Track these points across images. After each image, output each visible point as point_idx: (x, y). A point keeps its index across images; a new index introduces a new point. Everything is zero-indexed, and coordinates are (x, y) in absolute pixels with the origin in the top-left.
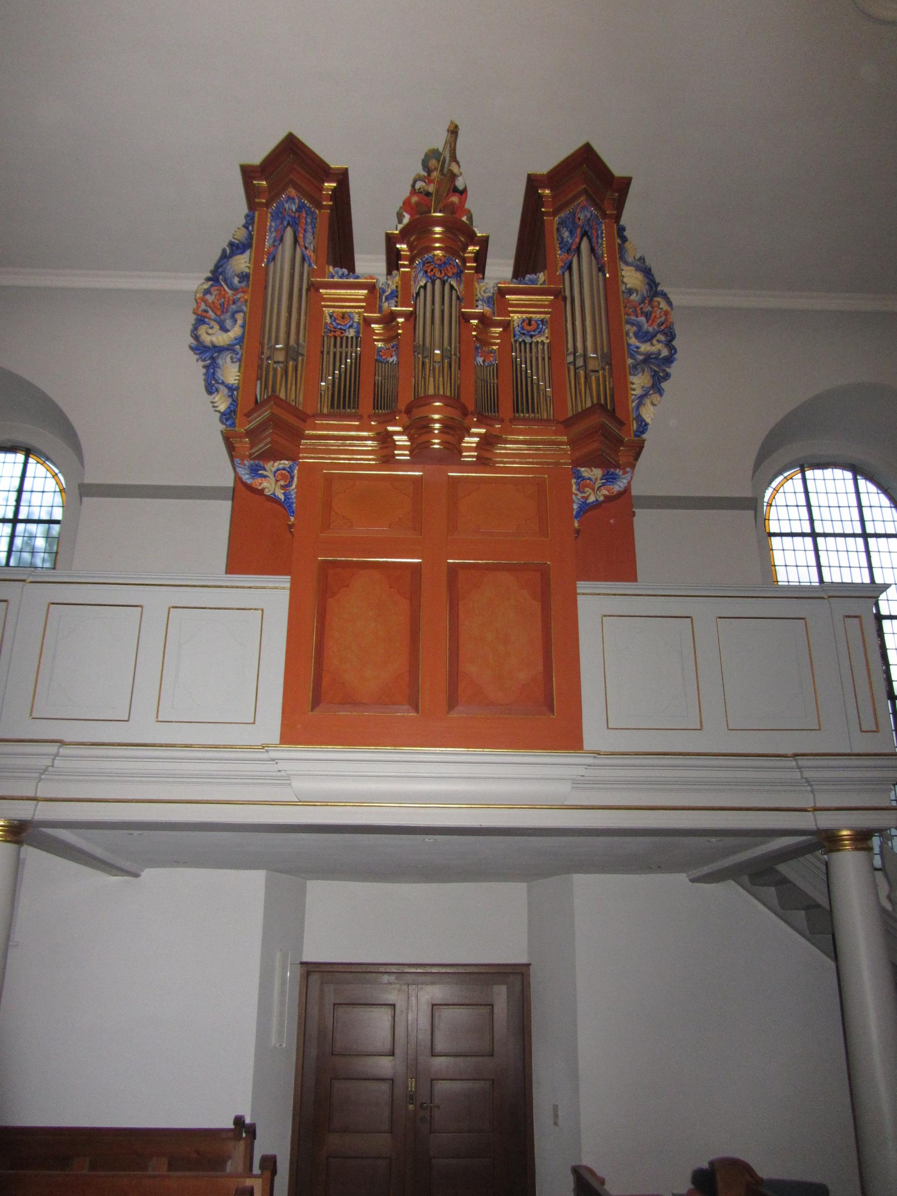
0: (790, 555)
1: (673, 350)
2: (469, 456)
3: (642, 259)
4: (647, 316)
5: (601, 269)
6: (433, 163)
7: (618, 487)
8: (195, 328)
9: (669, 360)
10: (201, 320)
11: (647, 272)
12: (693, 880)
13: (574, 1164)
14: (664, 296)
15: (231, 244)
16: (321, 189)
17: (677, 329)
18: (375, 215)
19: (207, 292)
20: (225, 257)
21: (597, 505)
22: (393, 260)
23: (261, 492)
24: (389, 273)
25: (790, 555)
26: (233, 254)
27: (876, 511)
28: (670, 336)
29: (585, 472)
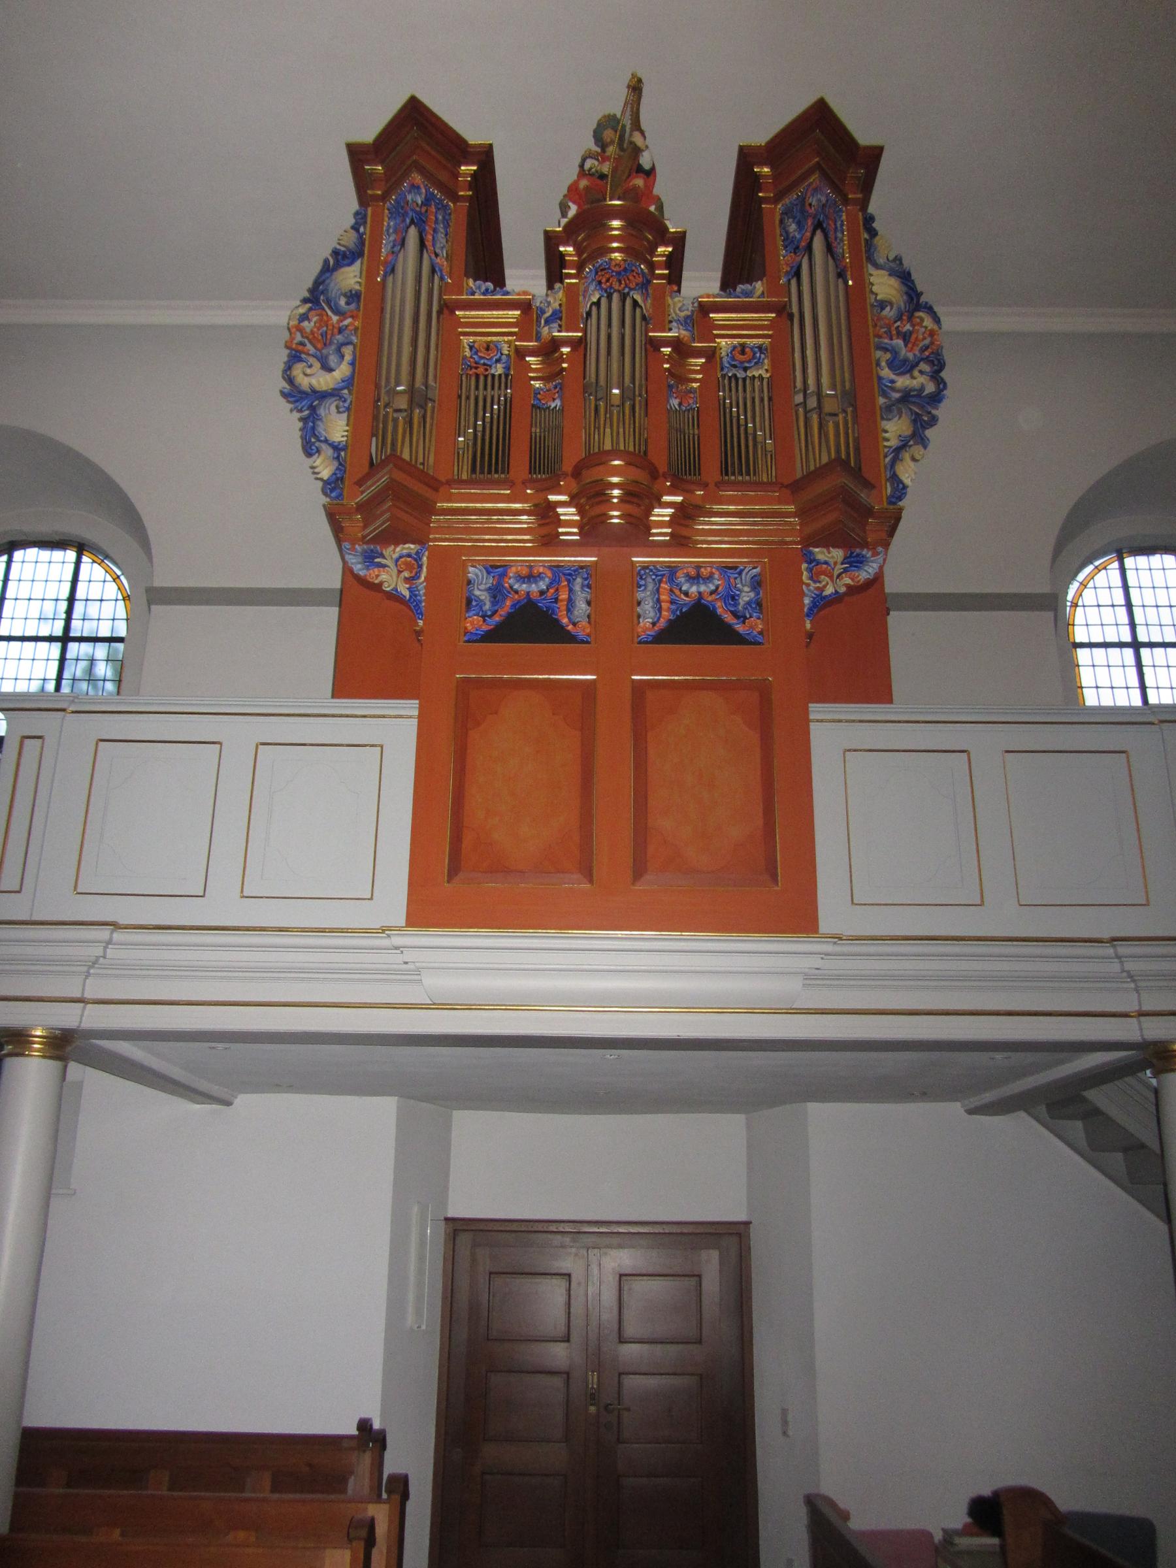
2: (660, 534)
3: (898, 259)
6: (608, 134)
8: (288, 368)
9: (936, 398)
10: (295, 357)
11: (905, 277)
12: (970, 1112)
14: (930, 310)
15: (335, 253)
17: (947, 356)
18: (529, 209)
19: (304, 317)
20: (327, 270)
21: (837, 598)
22: (555, 268)
23: (377, 587)
24: (550, 286)
26: (338, 265)
28: (937, 365)
29: (820, 553)
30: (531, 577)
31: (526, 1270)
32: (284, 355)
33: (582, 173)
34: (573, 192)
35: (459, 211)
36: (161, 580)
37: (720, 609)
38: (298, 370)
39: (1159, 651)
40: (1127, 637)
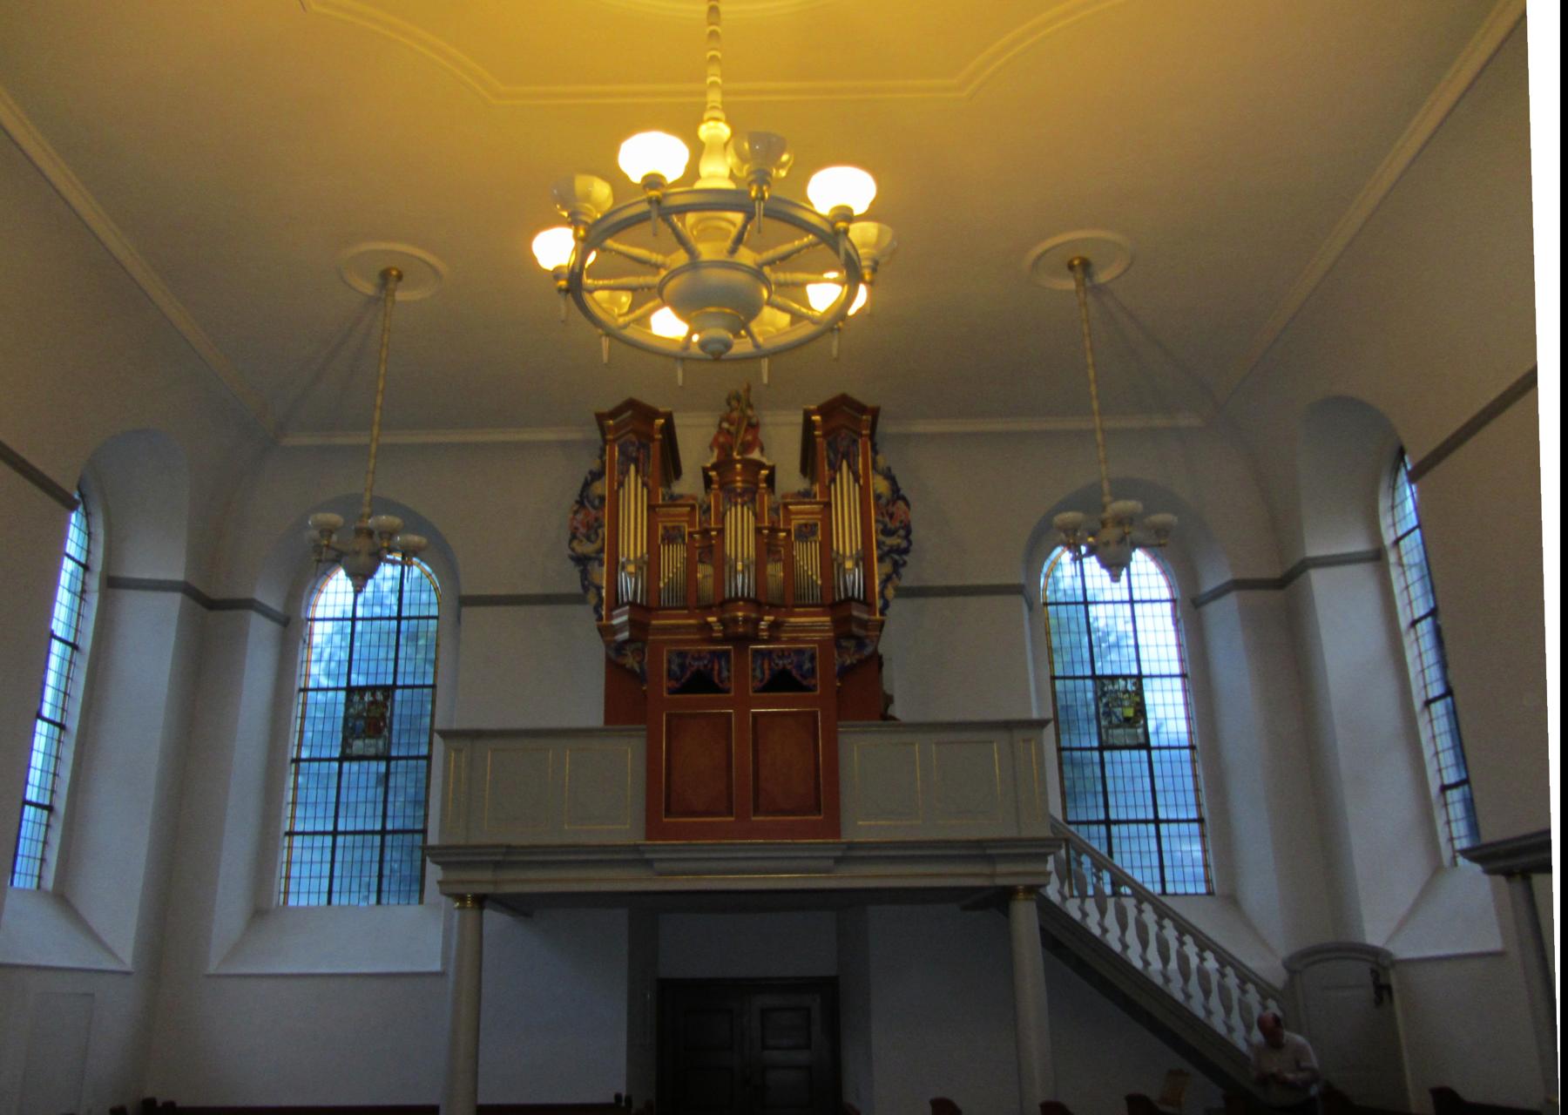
0: (1163, 656)
1: (910, 543)
2: (765, 635)
3: (889, 469)
4: (891, 516)
5: (857, 480)
6: (734, 403)
7: (869, 650)
8: (571, 541)
9: (906, 551)
10: (574, 537)
13: (932, 1096)
14: (904, 499)
15: (591, 472)
16: (652, 424)
17: (914, 526)
18: (696, 445)
20: (587, 485)
21: (852, 667)
22: (708, 482)
23: (623, 666)
25: (1163, 656)
26: (593, 480)
27: (1161, 641)
29: (844, 643)
30: (700, 658)
31: (538, 610)
32: (568, 536)
33: (721, 430)
34: (715, 443)
35: (655, 448)
36: (466, 591)
37: (794, 672)
38: (575, 544)
39: (1148, 606)
40: (1127, 598)
